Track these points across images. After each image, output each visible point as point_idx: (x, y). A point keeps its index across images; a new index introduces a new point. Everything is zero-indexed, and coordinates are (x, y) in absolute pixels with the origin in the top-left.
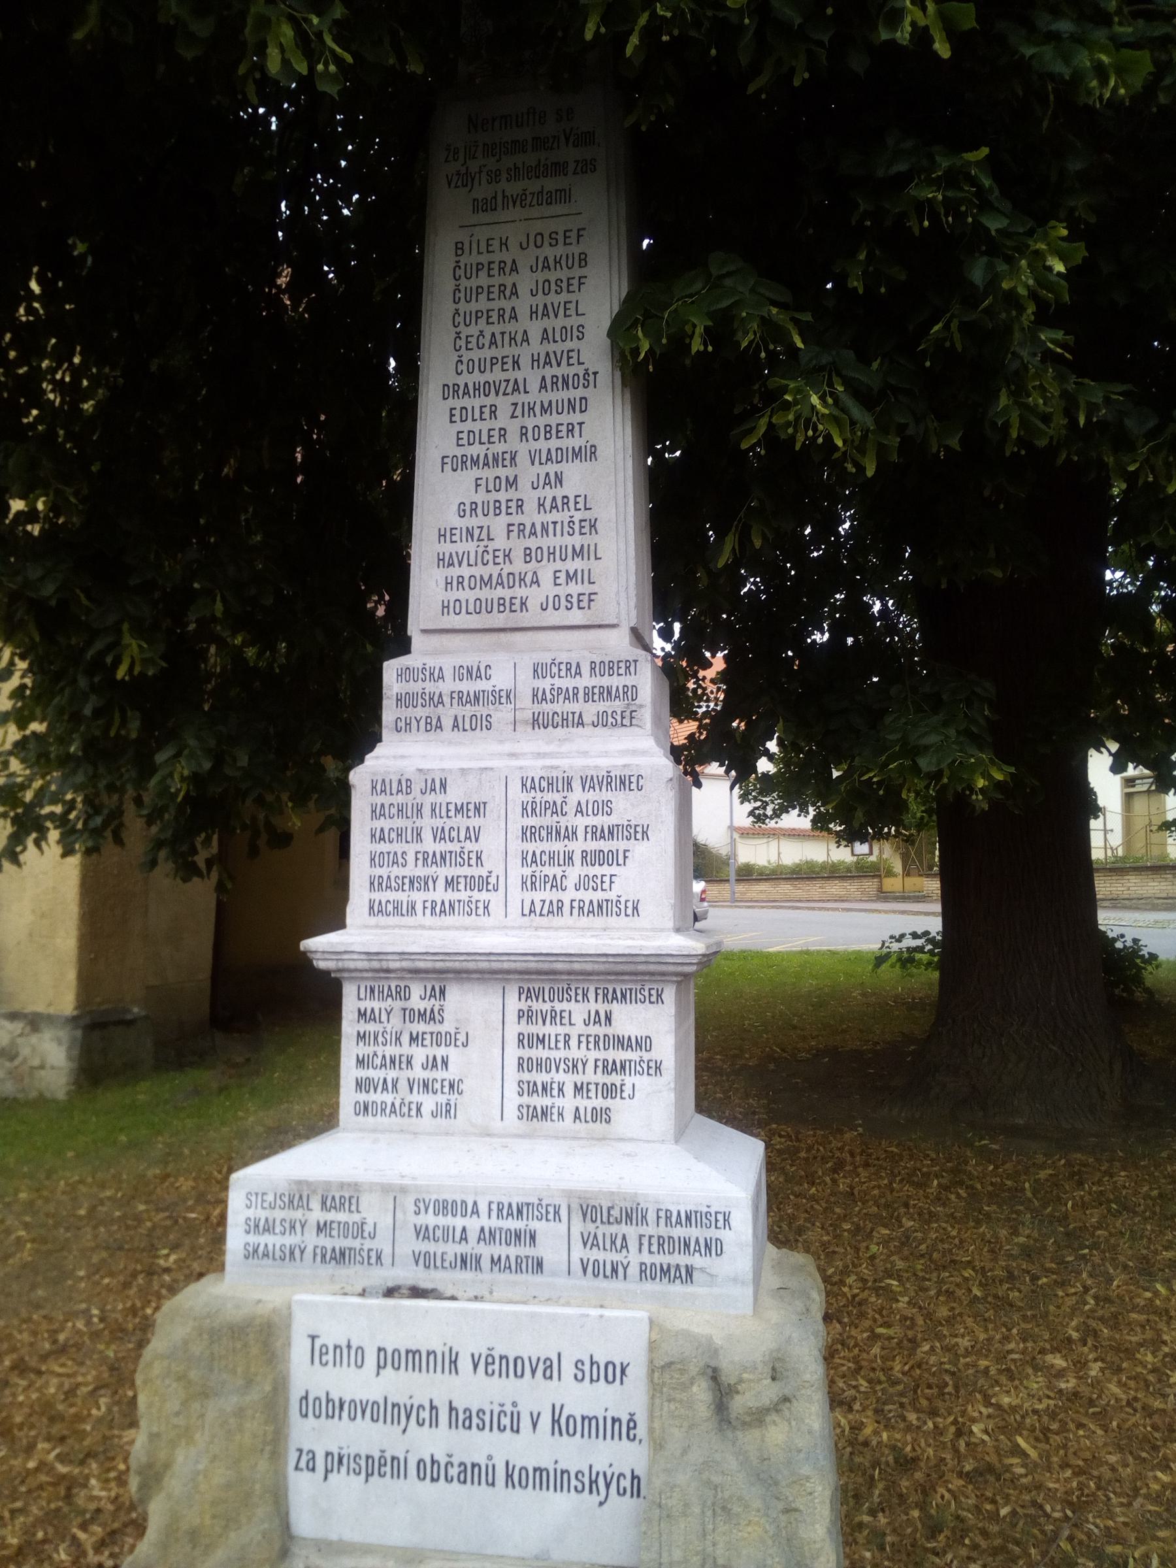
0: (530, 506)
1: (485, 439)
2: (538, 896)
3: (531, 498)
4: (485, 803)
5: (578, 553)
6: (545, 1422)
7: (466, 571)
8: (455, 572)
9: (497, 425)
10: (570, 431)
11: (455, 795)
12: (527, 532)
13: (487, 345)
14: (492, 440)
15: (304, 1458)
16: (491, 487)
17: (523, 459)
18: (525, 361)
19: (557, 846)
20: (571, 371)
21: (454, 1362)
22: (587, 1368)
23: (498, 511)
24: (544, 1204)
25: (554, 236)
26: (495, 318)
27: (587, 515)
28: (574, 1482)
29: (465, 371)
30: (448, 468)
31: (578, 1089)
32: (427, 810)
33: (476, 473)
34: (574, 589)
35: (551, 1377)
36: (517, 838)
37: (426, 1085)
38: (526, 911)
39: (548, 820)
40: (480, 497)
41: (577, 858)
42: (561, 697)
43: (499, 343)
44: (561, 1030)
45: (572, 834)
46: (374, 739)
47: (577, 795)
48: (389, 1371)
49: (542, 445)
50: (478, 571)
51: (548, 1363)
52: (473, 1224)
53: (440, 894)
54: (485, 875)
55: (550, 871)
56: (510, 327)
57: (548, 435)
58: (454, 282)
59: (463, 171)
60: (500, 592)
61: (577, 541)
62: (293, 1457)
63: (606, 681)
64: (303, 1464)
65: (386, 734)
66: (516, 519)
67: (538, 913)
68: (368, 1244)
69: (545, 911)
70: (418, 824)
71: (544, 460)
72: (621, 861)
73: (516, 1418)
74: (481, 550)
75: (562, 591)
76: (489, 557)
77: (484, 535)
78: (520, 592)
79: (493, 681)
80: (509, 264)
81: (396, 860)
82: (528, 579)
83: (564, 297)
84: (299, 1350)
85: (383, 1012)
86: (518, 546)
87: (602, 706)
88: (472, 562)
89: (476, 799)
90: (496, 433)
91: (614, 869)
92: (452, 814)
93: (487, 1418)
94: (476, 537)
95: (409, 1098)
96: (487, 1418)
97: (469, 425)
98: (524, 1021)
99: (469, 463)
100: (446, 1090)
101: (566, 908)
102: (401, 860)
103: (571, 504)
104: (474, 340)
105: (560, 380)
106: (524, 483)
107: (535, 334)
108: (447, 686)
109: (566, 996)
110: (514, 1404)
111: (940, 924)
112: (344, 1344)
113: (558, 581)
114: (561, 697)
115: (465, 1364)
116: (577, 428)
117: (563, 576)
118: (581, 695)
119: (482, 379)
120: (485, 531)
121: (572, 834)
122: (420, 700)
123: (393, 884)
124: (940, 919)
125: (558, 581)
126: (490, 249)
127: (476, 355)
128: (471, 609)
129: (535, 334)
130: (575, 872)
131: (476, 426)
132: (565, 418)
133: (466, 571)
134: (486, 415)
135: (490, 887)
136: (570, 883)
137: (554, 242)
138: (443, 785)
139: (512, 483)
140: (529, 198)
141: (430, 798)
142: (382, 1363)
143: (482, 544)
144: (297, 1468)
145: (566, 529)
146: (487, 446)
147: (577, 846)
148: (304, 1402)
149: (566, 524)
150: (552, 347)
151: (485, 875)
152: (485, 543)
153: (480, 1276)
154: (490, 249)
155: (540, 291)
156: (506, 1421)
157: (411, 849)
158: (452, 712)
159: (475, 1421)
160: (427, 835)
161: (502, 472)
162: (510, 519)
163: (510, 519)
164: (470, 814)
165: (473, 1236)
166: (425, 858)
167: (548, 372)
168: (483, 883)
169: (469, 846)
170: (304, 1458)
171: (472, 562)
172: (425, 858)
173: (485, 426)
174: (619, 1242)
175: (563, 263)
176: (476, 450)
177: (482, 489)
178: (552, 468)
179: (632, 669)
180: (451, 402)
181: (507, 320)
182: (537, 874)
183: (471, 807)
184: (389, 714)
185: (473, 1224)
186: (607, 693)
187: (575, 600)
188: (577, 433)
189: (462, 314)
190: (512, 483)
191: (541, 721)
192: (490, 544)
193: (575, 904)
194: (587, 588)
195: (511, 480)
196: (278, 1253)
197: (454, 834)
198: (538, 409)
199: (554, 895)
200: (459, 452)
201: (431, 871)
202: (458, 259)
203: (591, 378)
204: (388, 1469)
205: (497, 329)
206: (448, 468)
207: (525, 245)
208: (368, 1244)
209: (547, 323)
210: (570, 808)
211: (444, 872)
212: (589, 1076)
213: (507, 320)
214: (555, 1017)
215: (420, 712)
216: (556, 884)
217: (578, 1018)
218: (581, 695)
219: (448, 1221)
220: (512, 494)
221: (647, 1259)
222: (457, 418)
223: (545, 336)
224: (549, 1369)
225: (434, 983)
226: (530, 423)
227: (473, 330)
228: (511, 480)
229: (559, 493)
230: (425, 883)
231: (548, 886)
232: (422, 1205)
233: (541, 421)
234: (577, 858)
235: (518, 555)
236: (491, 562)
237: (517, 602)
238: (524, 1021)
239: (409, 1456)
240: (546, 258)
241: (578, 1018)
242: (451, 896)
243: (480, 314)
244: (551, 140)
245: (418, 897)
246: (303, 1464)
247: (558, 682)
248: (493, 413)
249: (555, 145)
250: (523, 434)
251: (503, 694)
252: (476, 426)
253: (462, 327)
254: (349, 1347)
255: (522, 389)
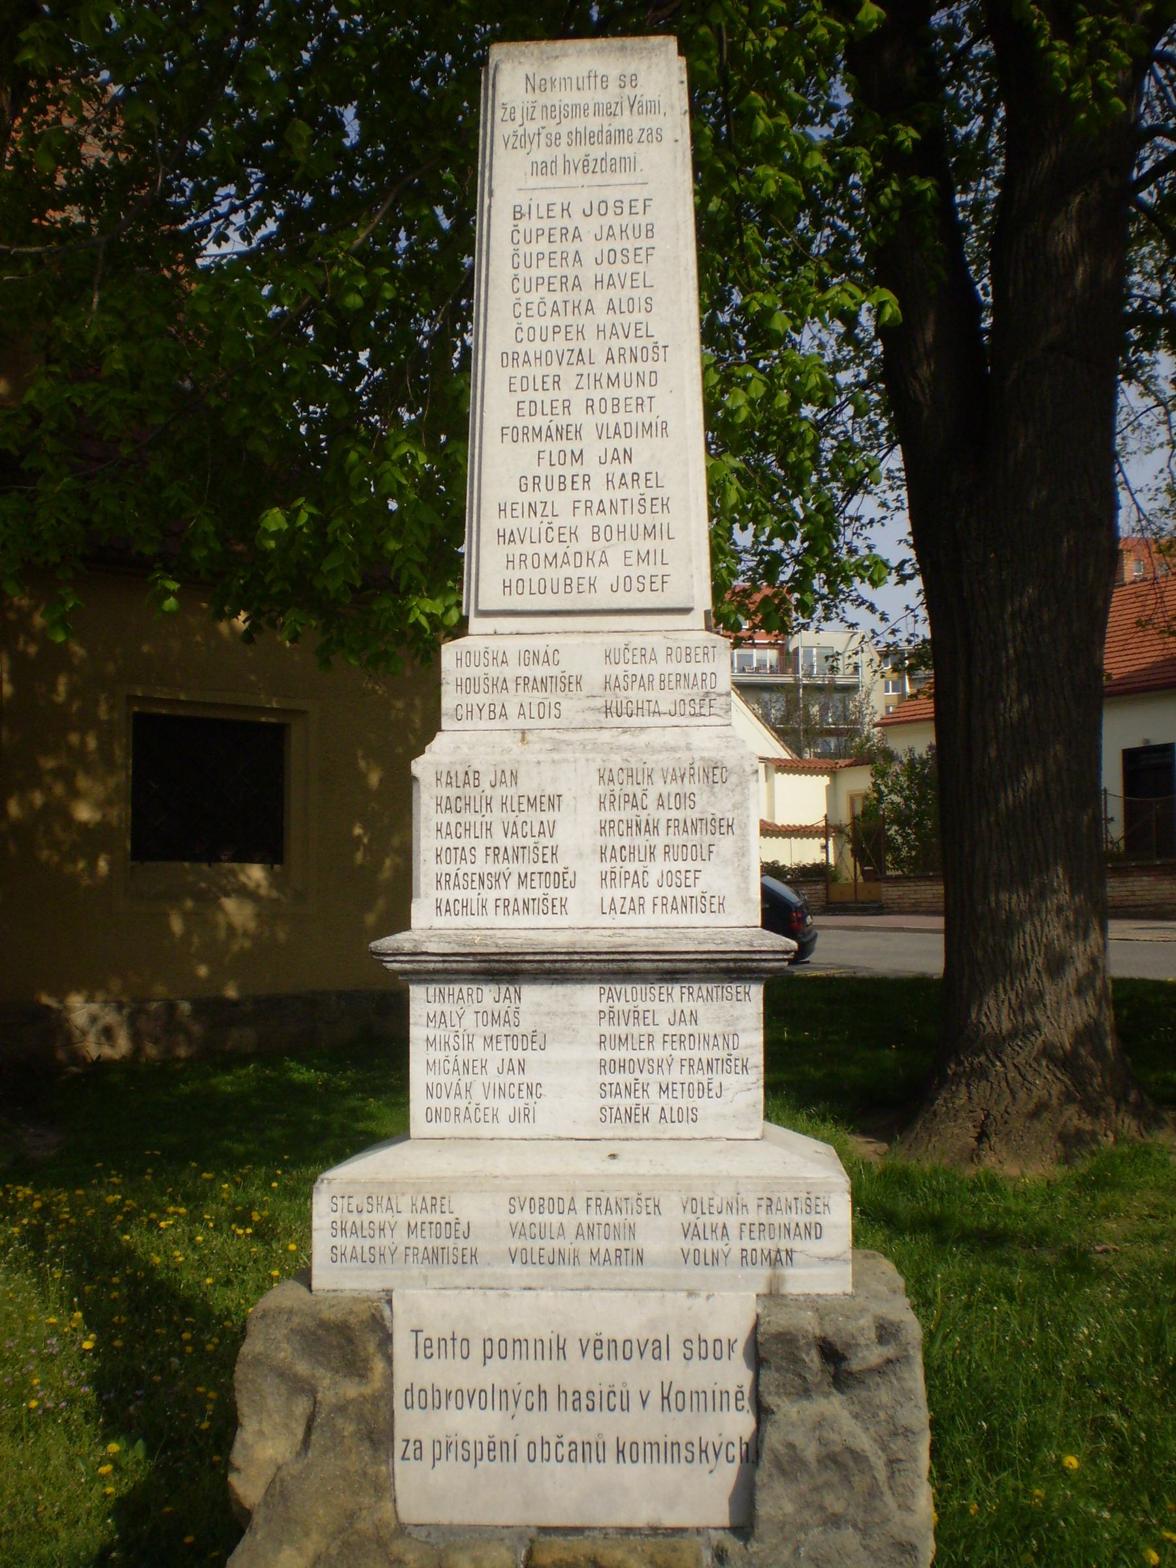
0: (598, 481)
1: (547, 410)
2: (618, 892)
3: (598, 475)
4: (559, 796)
5: (649, 532)
6: (655, 1398)
7: (528, 549)
8: (516, 549)
9: (561, 395)
10: (640, 404)
11: (528, 786)
12: (521, 361)
13: (549, 313)
14: (555, 411)
15: (411, 1447)
16: (555, 460)
17: (589, 433)
18: (590, 332)
19: (641, 841)
20: (640, 343)
21: (562, 1349)
22: (695, 1347)
23: (562, 487)
24: (643, 1198)
25: (618, 204)
26: (557, 286)
27: (657, 493)
28: (684, 1453)
29: (525, 339)
30: (508, 439)
31: (664, 1090)
32: (496, 805)
33: (538, 445)
34: (646, 570)
35: (660, 1357)
36: (595, 832)
37: (502, 1091)
38: (606, 910)
39: (628, 814)
40: (543, 470)
41: (659, 852)
42: (636, 685)
43: (562, 311)
44: (644, 1030)
45: (651, 828)
46: (432, 726)
47: (659, 787)
48: (495, 1362)
49: (610, 419)
50: (544, 548)
51: (657, 1344)
52: (569, 1221)
53: (511, 891)
54: (561, 871)
55: (631, 867)
56: (574, 296)
57: (616, 409)
58: (513, 246)
59: (520, 132)
60: (569, 571)
61: (647, 519)
62: (399, 1446)
63: (683, 668)
64: (410, 1453)
65: (446, 723)
66: (583, 495)
67: (618, 911)
68: (461, 1243)
69: (626, 909)
70: (488, 819)
71: (611, 434)
72: (705, 856)
73: (625, 1396)
74: (544, 527)
75: (634, 572)
76: (553, 534)
77: (548, 511)
78: (587, 571)
79: (561, 667)
80: (571, 231)
81: (462, 854)
82: (597, 559)
83: (631, 267)
84: (402, 1344)
85: (454, 1016)
86: (585, 523)
87: (678, 694)
88: (535, 538)
89: (550, 791)
90: (559, 404)
91: (698, 865)
92: (524, 807)
93: (597, 1399)
94: (539, 514)
95: (484, 1103)
96: (597, 1399)
97: (530, 395)
98: (605, 1022)
99: (530, 435)
100: (524, 1093)
101: (648, 905)
102: (469, 857)
103: (642, 481)
104: (535, 307)
105: (628, 352)
106: (591, 457)
107: (600, 303)
108: (511, 671)
109: (649, 995)
110: (625, 1384)
111: (938, 943)
112: (448, 1337)
113: (628, 561)
114: (636, 685)
115: (573, 1350)
116: (647, 402)
117: (634, 556)
118: (656, 682)
119: (544, 347)
120: (549, 506)
121: (651, 828)
122: (482, 686)
123: (462, 882)
124: (941, 937)
125: (628, 561)
126: (551, 214)
127: (537, 322)
128: (535, 589)
129: (600, 303)
130: (657, 868)
131: (539, 396)
132: (634, 392)
133: (528, 549)
134: (549, 385)
135: (567, 884)
136: (652, 878)
137: (618, 204)
138: (514, 775)
139: (578, 457)
140: (592, 165)
141: (501, 791)
142: (488, 1353)
143: (546, 520)
144: (403, 1458)
145: (636, 507)
146: (550, 417)
147: (660, 841)
148: (409, 1393)
149: (636, 502)
150: (619, 319)
151: (561, 871)
152: (550, 519)
153: (578, 1269)
154: (551, 214)
155: (606, 260)
156: (616, 1401)
157: (481, 845)
158: (517, 700)
159: (584, 1402)
160: (498, 830)
161: (568, 446)
162: (576, 495)
163: (576, 495)
164: (545, 807)
165: (571, 1230)
166: (495, 852)
167: (615, 343)
168: (560, 879)
169: (545, 841)
170: (411, 1447)
171: (535, 538)
172: (495, 852)
173: (547, 397)
174: (719, 1231)
175: (630, 232)
176: (539, 421)
177: (545, 462)
178: (620, 443)
179: (710, 655)
180: (510, 371)
181: (570, 288)
182: (617, 870)
183: (545, 800)
184: (450, 699)
185: (569, 1221)
186: (683, 678)
187: (647, 582)
188: (646, 408)
189: (522, 281)
190: (578, 457)
191: (614, 710)
192: (555, 520)
193: (658, 901)
194: (660, 570)
195: (577, 453)
196: (367, 1256)
197: (527, 829)
198: (604, 380)
199: (636, 892)
200: (520, 422)
201: (502, 867)
202: (516, 222)
203: (661, 352)
204: (498, 1453)
205: (559, 297)
206: (508, 439)
207: (588, 212)
208: (461, 1243)
209: (612, 293)
210: (651, 801)
211: (518, 868)
212: (676, 1075)
213: (570, 288)
214: (637, 1016)
215: (482, 699)
216: (637, 879)
217: (663, 1019)
218: (656, 682)
219: (546, 1218)
220: (577, 468)
221: (748, 1244)
222: (517, 387)
223: (611, 308)
224: (658, 1349)
225: (442, 986)
226: (596, 395)
227: (534, 297)
228: (577, 453)
229: (628, 468)
230: (498, 879)
231: (629, 882)
232: (517, 1204)
233: (610, 393)
234: (659, 852)
235: (585, 533)
236: (556, 539)
237: (585, 582)
238: (605, 1022)
239: (518, 1439)
240: (611, 227)
241: (663, 1019)
242: (525, 893)
243: (540, 281)
244: (613, 106)
245: (491, 895)
246: (410, 1453)
247: (632, 669)
248: (557, 383)
249: (618, 111)
250: (590, 405)
251: (573, 680)
252: (539, 396)
253: (521, 293)
254: (453, 1339)
255: (586, 359)
